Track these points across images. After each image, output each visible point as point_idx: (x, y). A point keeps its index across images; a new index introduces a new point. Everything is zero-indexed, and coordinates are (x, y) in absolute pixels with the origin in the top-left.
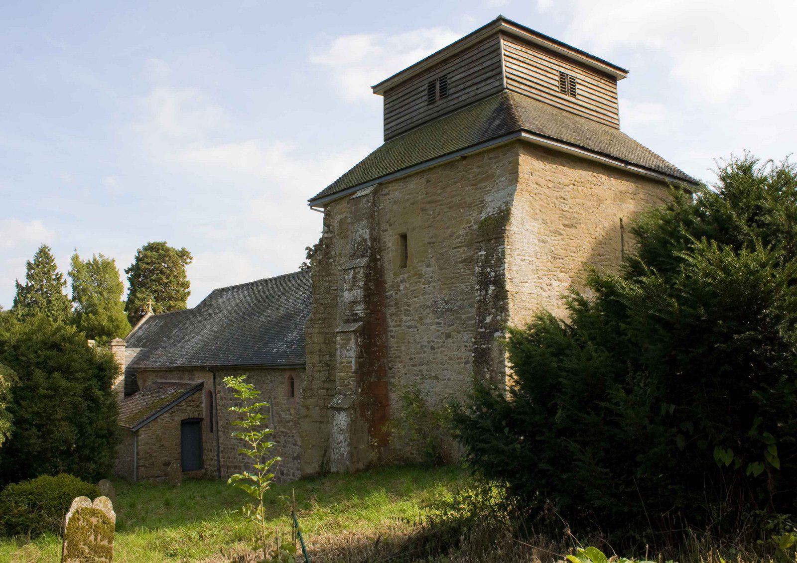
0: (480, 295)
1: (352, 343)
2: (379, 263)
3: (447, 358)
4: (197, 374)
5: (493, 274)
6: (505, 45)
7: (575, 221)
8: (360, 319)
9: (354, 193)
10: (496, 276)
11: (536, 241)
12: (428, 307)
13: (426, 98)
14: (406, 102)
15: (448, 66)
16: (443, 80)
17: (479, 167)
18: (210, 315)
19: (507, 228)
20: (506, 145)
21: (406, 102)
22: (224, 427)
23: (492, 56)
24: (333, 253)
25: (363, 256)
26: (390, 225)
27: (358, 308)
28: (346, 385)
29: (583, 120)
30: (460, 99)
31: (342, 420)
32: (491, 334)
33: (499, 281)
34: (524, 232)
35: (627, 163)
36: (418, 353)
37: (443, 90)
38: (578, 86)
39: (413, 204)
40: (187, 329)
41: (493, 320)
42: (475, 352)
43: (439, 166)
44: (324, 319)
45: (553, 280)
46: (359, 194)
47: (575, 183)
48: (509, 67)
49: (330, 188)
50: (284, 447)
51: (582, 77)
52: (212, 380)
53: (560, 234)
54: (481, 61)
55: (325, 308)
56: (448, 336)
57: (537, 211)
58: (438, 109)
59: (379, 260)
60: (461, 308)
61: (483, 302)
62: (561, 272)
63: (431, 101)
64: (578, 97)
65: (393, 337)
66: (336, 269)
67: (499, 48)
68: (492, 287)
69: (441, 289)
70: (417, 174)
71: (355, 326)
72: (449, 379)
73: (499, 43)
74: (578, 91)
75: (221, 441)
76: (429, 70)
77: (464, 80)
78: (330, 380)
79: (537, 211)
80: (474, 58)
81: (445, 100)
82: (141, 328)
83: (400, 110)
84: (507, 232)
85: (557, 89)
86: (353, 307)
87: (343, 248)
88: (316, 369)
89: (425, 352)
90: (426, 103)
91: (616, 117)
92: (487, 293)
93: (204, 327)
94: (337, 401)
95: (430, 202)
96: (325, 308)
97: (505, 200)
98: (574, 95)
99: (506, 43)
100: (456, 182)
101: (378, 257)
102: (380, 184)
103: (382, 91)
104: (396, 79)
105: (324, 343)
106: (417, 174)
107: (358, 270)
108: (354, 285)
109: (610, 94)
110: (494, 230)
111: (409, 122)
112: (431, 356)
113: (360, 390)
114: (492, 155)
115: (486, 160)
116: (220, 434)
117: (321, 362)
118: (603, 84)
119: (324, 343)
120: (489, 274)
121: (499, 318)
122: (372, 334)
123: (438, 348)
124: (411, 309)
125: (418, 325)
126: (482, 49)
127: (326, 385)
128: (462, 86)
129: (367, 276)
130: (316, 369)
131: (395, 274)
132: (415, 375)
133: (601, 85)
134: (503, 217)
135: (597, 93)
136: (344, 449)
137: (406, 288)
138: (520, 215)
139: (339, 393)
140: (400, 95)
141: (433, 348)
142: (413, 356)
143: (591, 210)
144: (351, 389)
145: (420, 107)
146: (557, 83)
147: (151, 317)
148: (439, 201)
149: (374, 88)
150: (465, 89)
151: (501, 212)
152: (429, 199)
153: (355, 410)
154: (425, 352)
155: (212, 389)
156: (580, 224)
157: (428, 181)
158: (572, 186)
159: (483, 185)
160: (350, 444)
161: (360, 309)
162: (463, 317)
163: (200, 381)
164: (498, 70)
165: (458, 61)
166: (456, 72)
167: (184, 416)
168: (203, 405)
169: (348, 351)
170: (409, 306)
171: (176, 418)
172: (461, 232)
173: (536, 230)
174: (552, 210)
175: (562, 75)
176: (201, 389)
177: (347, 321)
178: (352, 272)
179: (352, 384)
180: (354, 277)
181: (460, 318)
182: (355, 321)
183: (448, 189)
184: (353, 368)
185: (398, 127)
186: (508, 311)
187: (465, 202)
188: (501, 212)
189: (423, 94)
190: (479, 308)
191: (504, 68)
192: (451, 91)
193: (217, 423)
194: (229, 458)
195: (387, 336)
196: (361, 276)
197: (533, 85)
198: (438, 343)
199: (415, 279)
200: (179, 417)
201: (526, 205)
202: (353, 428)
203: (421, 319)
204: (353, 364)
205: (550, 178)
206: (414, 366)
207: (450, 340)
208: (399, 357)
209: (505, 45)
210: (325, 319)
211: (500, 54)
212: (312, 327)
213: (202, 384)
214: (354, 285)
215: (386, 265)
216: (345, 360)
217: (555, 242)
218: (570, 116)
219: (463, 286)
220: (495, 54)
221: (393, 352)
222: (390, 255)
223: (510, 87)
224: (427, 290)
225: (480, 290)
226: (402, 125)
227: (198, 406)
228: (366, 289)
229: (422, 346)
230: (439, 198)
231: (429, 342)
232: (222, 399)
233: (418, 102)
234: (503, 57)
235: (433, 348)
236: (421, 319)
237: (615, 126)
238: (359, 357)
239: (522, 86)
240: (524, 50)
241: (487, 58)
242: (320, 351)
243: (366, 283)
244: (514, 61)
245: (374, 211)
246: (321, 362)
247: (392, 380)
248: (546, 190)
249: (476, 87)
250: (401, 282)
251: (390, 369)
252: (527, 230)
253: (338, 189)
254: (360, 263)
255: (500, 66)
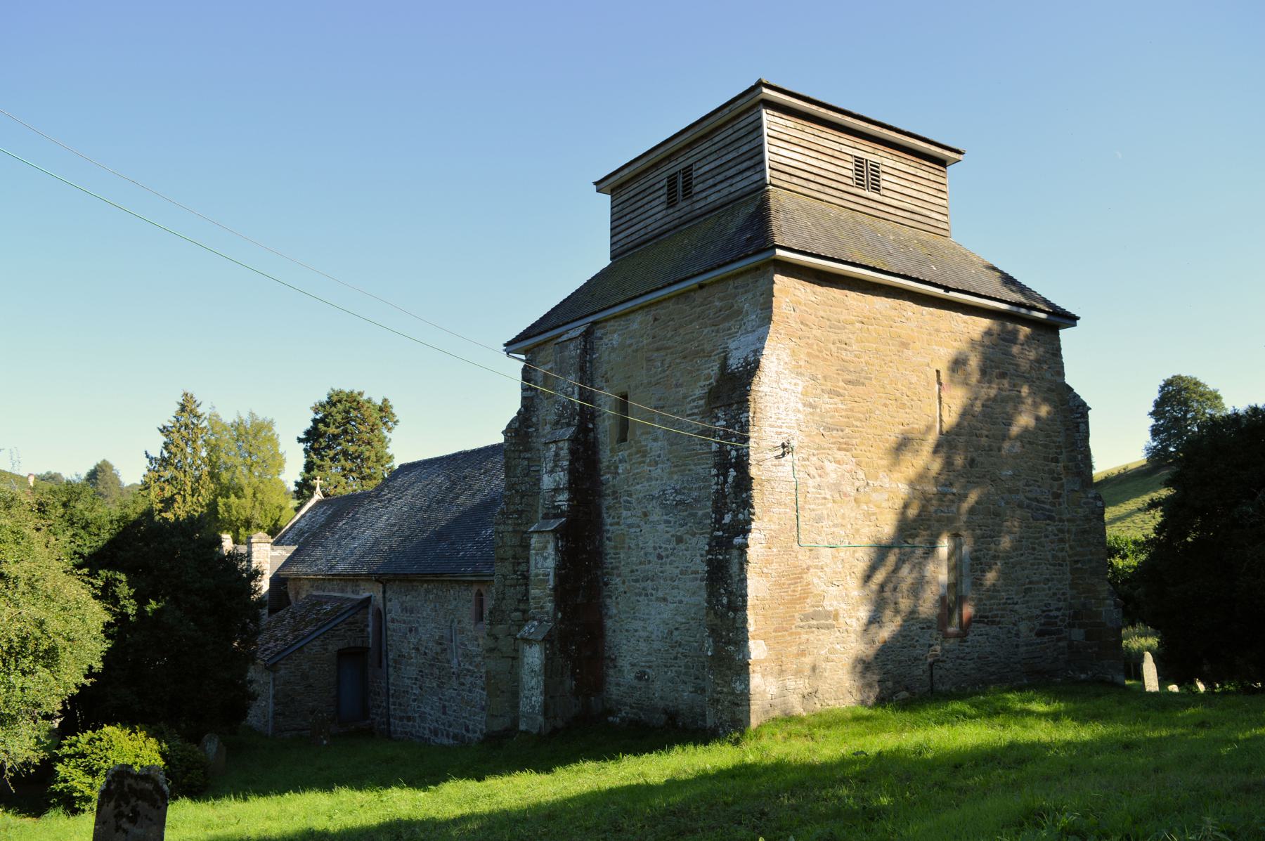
0: (717, 484)
1: (551, 549)
2: (592, 434)
3: (678, 571)
4: (363, 585)
5: (734, 453)
6: (769, 118)
7: (863, 374)
8: (562, 515)
9: (560, 335)
10: (738, 457)
11: (800, 406)
12: (653, 497)
13: (663, 198)
14: (639, 204)
15: (693, 153)
16: (687, 171)
17: (721, 299)
18: (390, 500)
19: (753, 387)
20: (757, 268)
21: (639, 204)
22: (395, 661)
23: (751, 137)
24: (534, 420)
25: (568, 425)
26: (607, 381)
27: (561, 498)
28: (542, 607)
29: (889, 226)
30: (709, 200)
31: (534, 657)
32: (731, 539)
33: (742, 464)
34: (782, 393)
35: (947, 289)
36: (641, 563)
37: (688, 186)
38: (883, 176)
39: (636, 351)
40: (357, 520)
41: (733, 520)
42: (708, 565)
43: (670, 298)
44: (520, 513)
45: (826, 463)
46: (565, 338)
47: (865, 320)
48: (772, 151)
49: (533, 326)
50: (470, 691)
51: (891, 163)
52: (381, 595)
53: (839, 395)
54: (736, 145)
55: (522, 498)
56: (680, 540)
57: (802, 363)
58: (677, 215)
59: (592, 430)
60: (697, 500)
61: (720, 494)
62: (839, 449)
63: (671, 203)
64: (883, 192)
65: (609, 539)
66: (537, 443)
67: (760, 126)
68: (732, 472)
69: (671, 473)
70: (641, 308)
71: (554, 524)
72: (681, 602)
73: (760, 118)
74: (883, 184)
75: (391, 680)
76: (668, 158)
77: (715, 172)
78: (525, 598)
79: (802, 363)
80: (728, 141)
81: (689, 202)
82: (303, 516)
83: (632, 215)
84: (753, 393)
85: (850, 182)
86: (553, 496)
87: (547, 413)
88: (508, 582)
89: (649, 562)
90: (664, 206)
91: (945, 218)
92: (725, 481)
93: (381, 516)
94: (528, 629)
95: (658, 350)
96: (522, 498)
97: (753, 348)
98: (876, 189)
99: (770, 118)
100: (691, 322)
101: (591, 426)
102: (594, 323)
103: (609, 189)
104: (626, 171)
105: (520, 546)
106: (641, 308)
107: (561, 444)
108: (556, 466)
109: (935, 185)
110: (733, 390)
111: (642, 232)
112: (658, 569)
113: (560, 615)
114: (739, 282)
115: (731, 290)
116: (391, 669)
117: (515, 572)
118: (924, 170)
119: (520, 546)
120: (729, 452)
121: (741, 516)
122: (582, 535)
123: (667, 557)
124: (633, 500)
125: (642, 523)
126: (736, 127)
127: (522, 606)
128: (711, 182)
129: (572, 452)
130: (508, 582)
131: (612, 450)
132: (637, 594)
133: (920, 173)
134: (751, 368)
135: (914, 186)
136: (537, 699)
137: (627, 471)
138: (774, 369)
139: (534, 619)
140: (632, 194)
141: (660, 557)
142: (635, 568)
143: (889, 359)
144: (547, 613)
145: (656, 214)
146: (850, 174)
147: (319, 502)
148: (669, 348)
149: (596, 183)
150: (715, 185)
151: (748, 364)
152: (655, 345)
153: (552, 643)
154: (649, 562)
155: (381, 606)
156: (870, 379)
157: (655, 320)
158: (858, 325)
159: (727, 325)
160: (546, 692)
161: (563, 499)
162: (700, 513)
163: (366, 595)
164: (758, 158)
165: (707, 145)
166: (704, 162)
167: (342, 645)
168: (370, 629)
169: (545, 558)
170: (630, 495)
171: (330, 647)
172: (698, 392)
173: (800, 389)
174: (825, 360)
175: (859, 161)
176: (367, 607)
177: (546, 516)
178: (553, 447)
179: (549, 606)
180: (557, 455)
181: (694, 515)
182: (556, 516)
183: (681, 331)
184: (551, 584)
185: (630, 239)
186: (752, 507)
187: (703, 350)
188: (748, 364)
189: (661, 192)
190: (715, 502)
191: (767, 155)
192: (697, 189)
193: (387, 656)
194: (400, 705)
195: (602, 537)
196: (564, 453)
197: (812, 177)
198: (666, 549)
199: (636, 458)
200: (334, 647)
201: (785, 356)
202: (549, 668)
203: (645, 514)
204: (551, 577)
205: (822, 314)
206: (637, 581)
207: (682, 546)
208: (617, 568)
209: (769, 118)
210: (522, 511)
211: (762, 135)
212: (504, 523)
213: (369, 599)
214: (556, 466)
215: (601, 437)
216: (541, 572)
217: (827, 403)
218: (866, 219)
219: (699, 469)
220: (755, 134)
221: (609, 561)
222: (607, 423)
223: (774, 182)
224: (654, 474)
225: (717, 476)
226: (634, 237)
227: (362, 631)
228: (572, 471)
229: (646, 554)
230: (670, 343)
231: (655, 548)
232: (393, 621)
233: (654, 203)
234: (766, 139)
235: (660, 557)
236: (645, 514)
237: (944, 233)
238: (558, 568)
239: (795, 180)
240: (799, 127)
241: (745, 141)
242: (514, 557)
243: (571, 463)
244: (782, 141)
245: (585, 362)
246: (515, 572)
247: (608, 601)
248: (818, 333)
249: (729, 182)
250: (620, 461)
251: (606, 584)
252: (785, 390)
253: (543, 327)
254: (564, 434)
255: (762, 152)
